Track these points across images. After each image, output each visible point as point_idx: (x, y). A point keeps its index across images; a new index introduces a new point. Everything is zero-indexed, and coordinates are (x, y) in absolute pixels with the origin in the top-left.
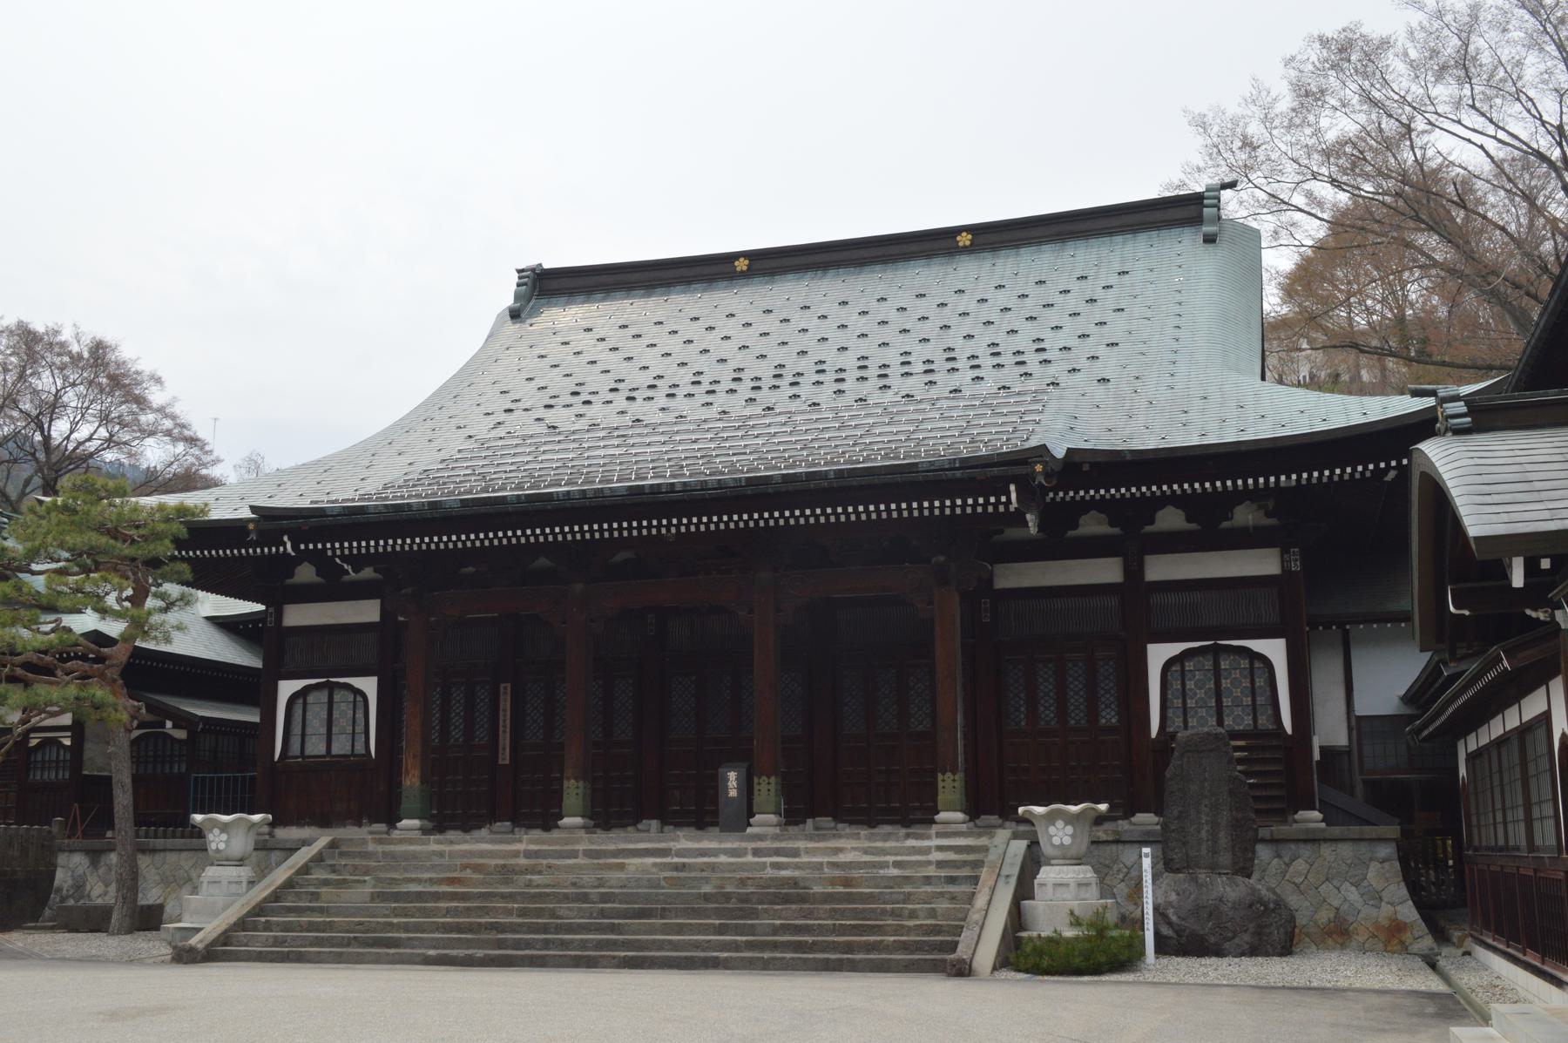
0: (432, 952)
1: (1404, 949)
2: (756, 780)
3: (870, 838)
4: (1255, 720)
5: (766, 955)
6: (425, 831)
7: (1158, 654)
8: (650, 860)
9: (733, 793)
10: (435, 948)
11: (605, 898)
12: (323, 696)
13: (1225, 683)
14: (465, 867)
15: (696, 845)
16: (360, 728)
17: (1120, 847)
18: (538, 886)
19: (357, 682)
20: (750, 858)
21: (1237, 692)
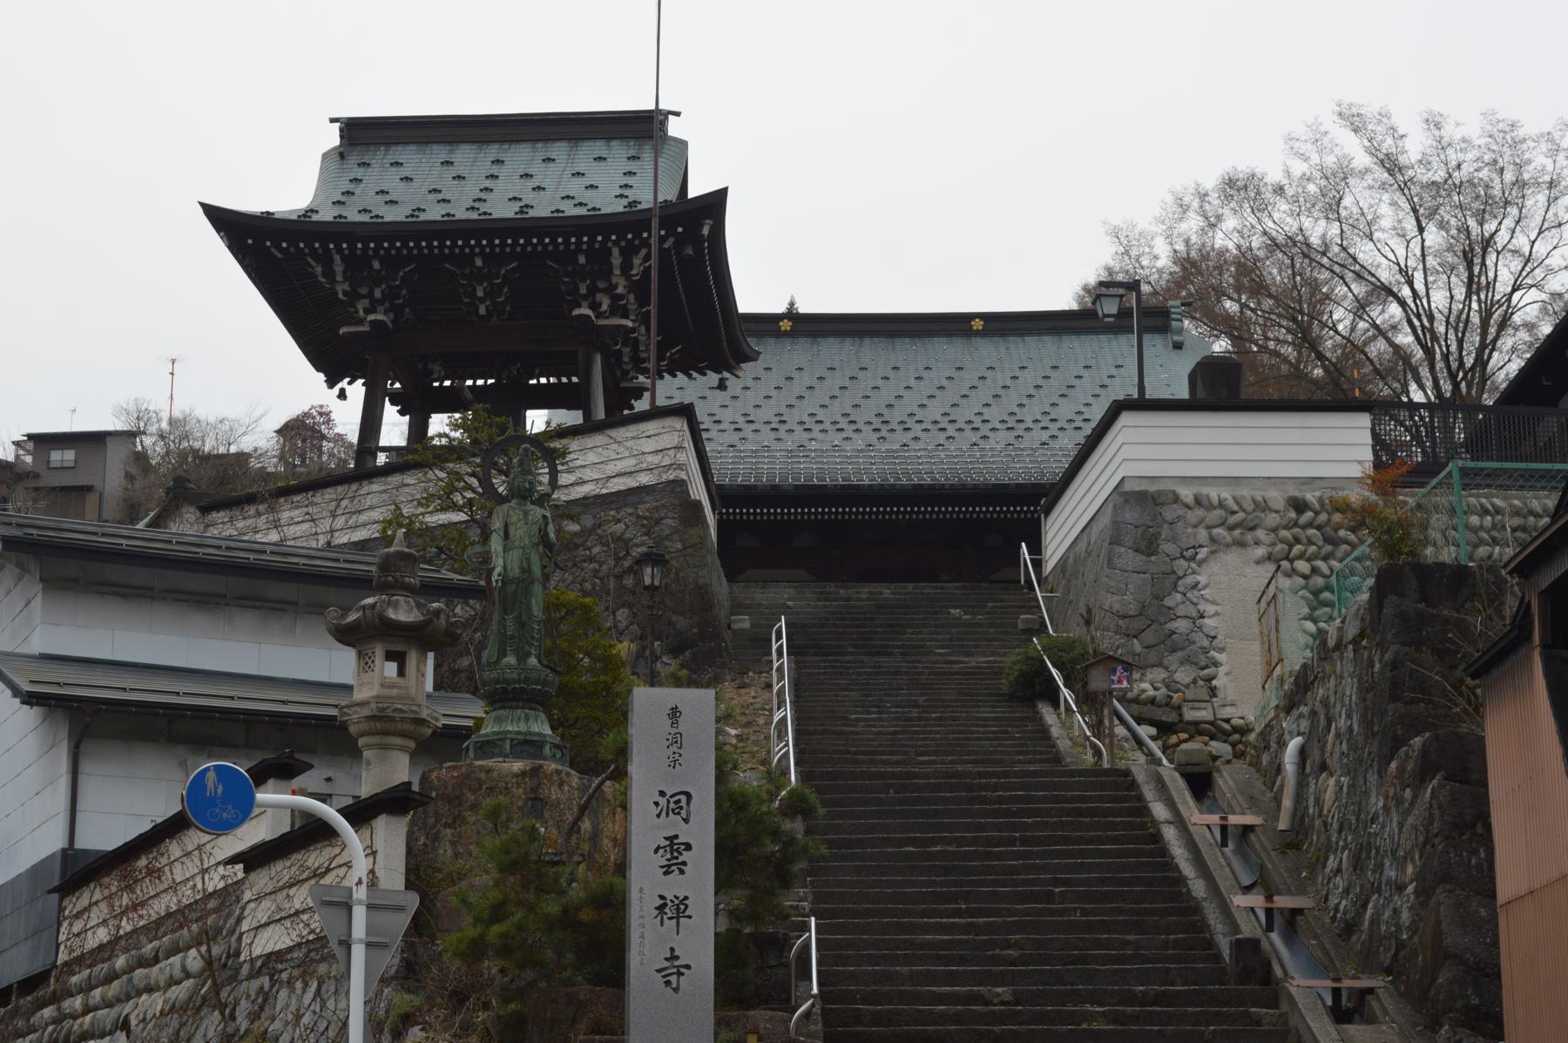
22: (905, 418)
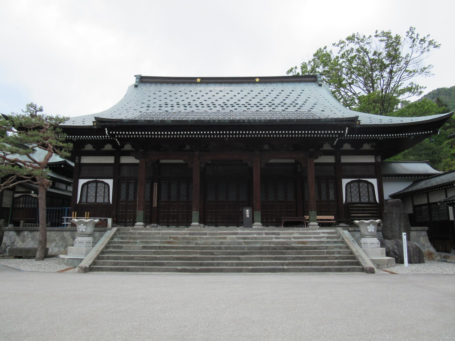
0: (179, 268)
1: (433, 259)
2: (255, 212)
3: (298, 230)
4: (369, 199)
5: (301, 267)
6: (145, 226)
7: (345, 181)
8: (235, 236)
9: (248, 216)
10: (181, 266)
11: (226, 248)
12: (94, 185)
13: (361, 190)
14: (170, 238)
15: (243, 232)
16: (106, 195)
17: (355, 232)
18: (200, 244)
19: (106, 181)
20: (264, 236)
21: (364, 192)
22: (233, 103)
